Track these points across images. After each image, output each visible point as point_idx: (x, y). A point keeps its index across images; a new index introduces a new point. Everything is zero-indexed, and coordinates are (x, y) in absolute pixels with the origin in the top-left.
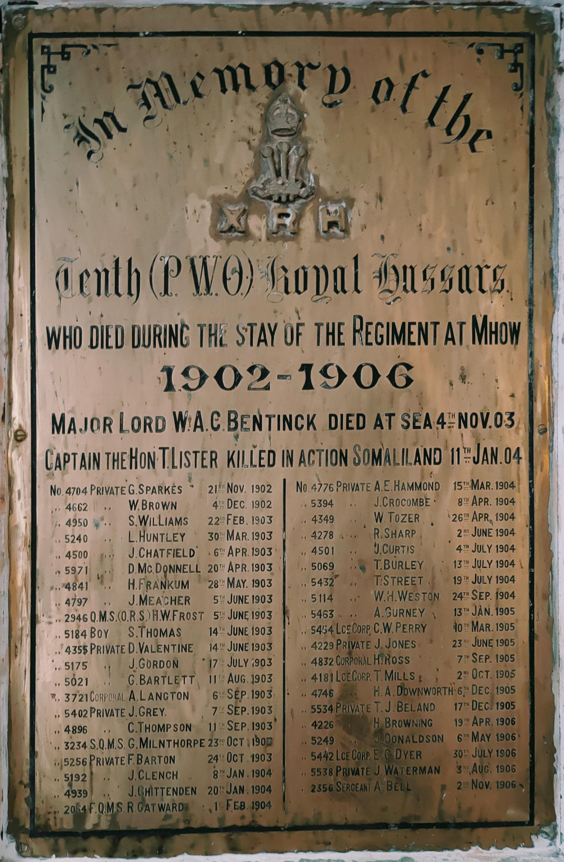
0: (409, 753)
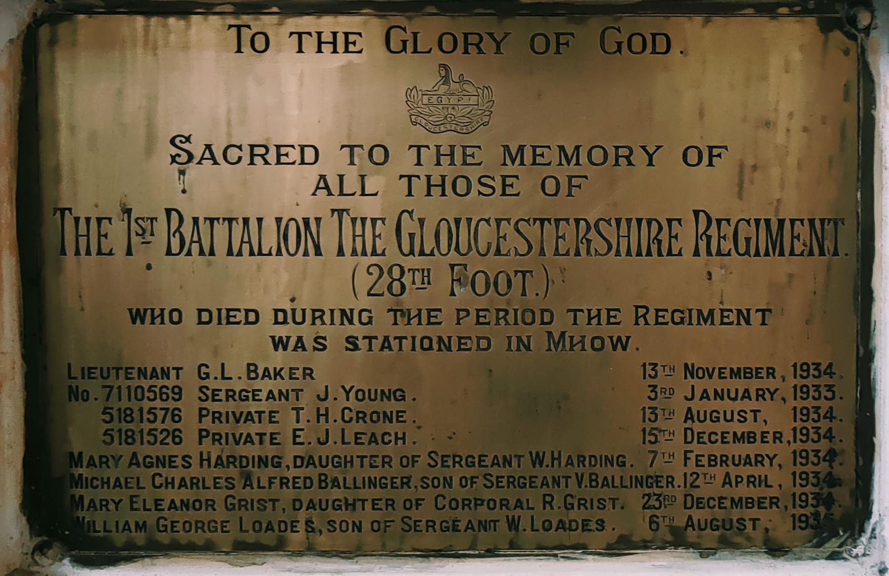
0: (717, 371)
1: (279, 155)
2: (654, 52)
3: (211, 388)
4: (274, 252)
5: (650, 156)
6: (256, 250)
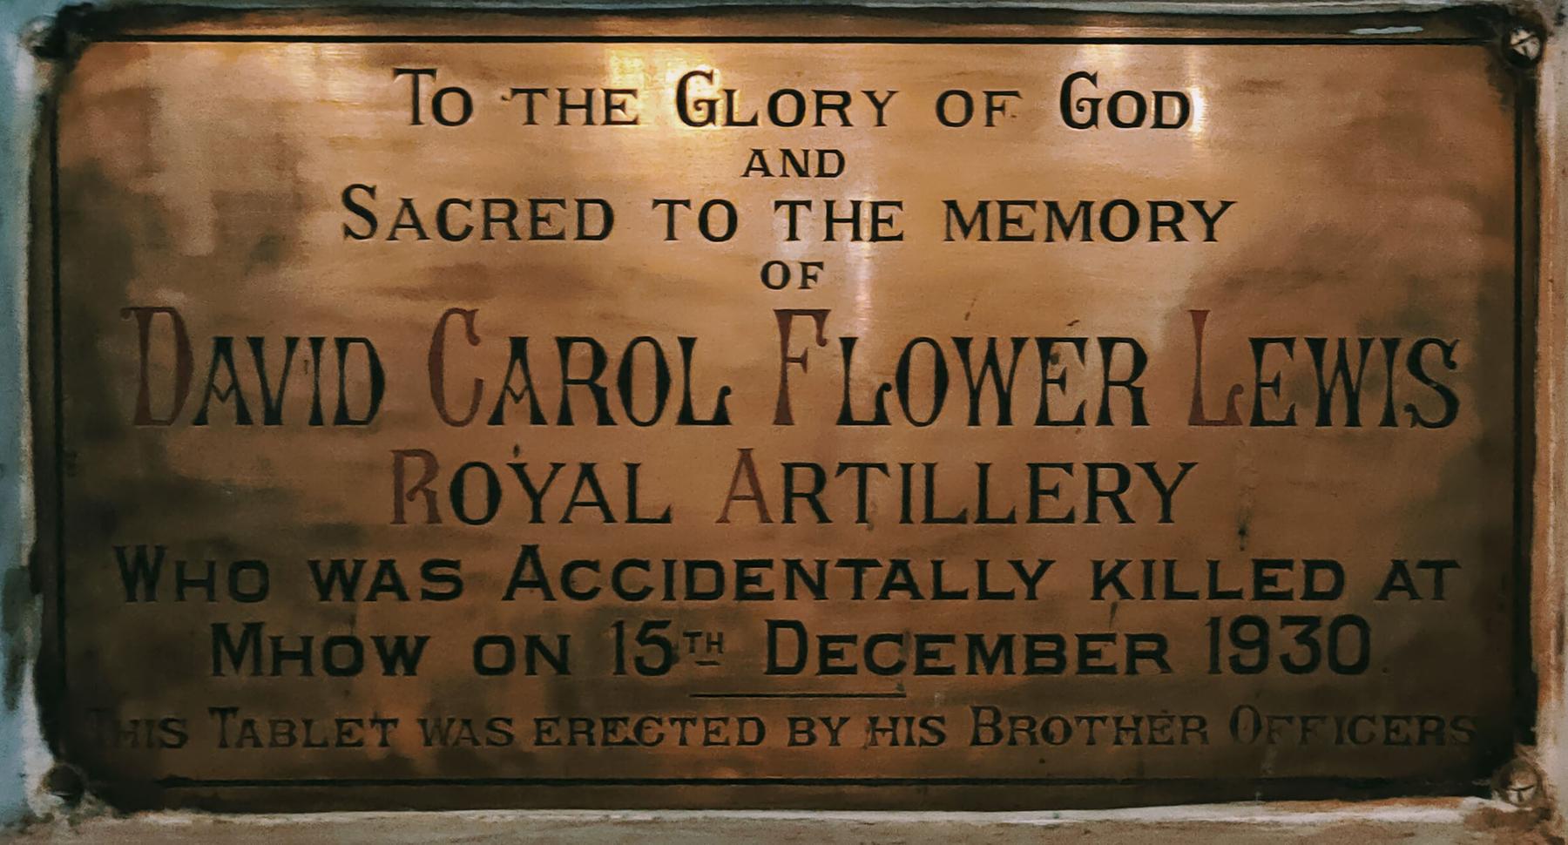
1: (535, 219)
2: (1159, 124)
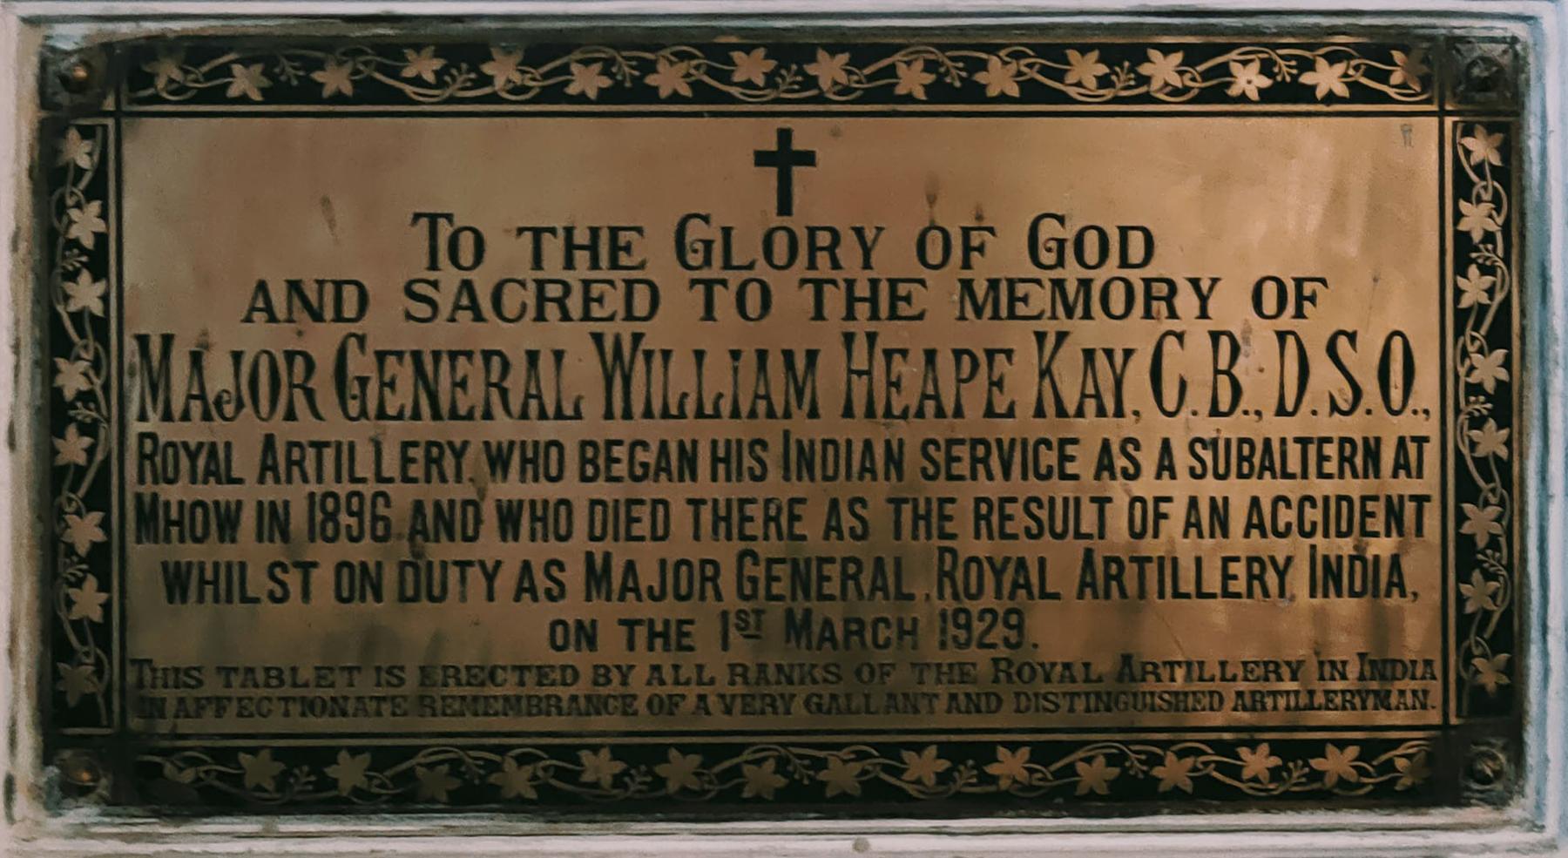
1: (587, 300)
3: (1243, 555)
4: (478, 413)
5: (1204, 300)
6: (551, 410)
